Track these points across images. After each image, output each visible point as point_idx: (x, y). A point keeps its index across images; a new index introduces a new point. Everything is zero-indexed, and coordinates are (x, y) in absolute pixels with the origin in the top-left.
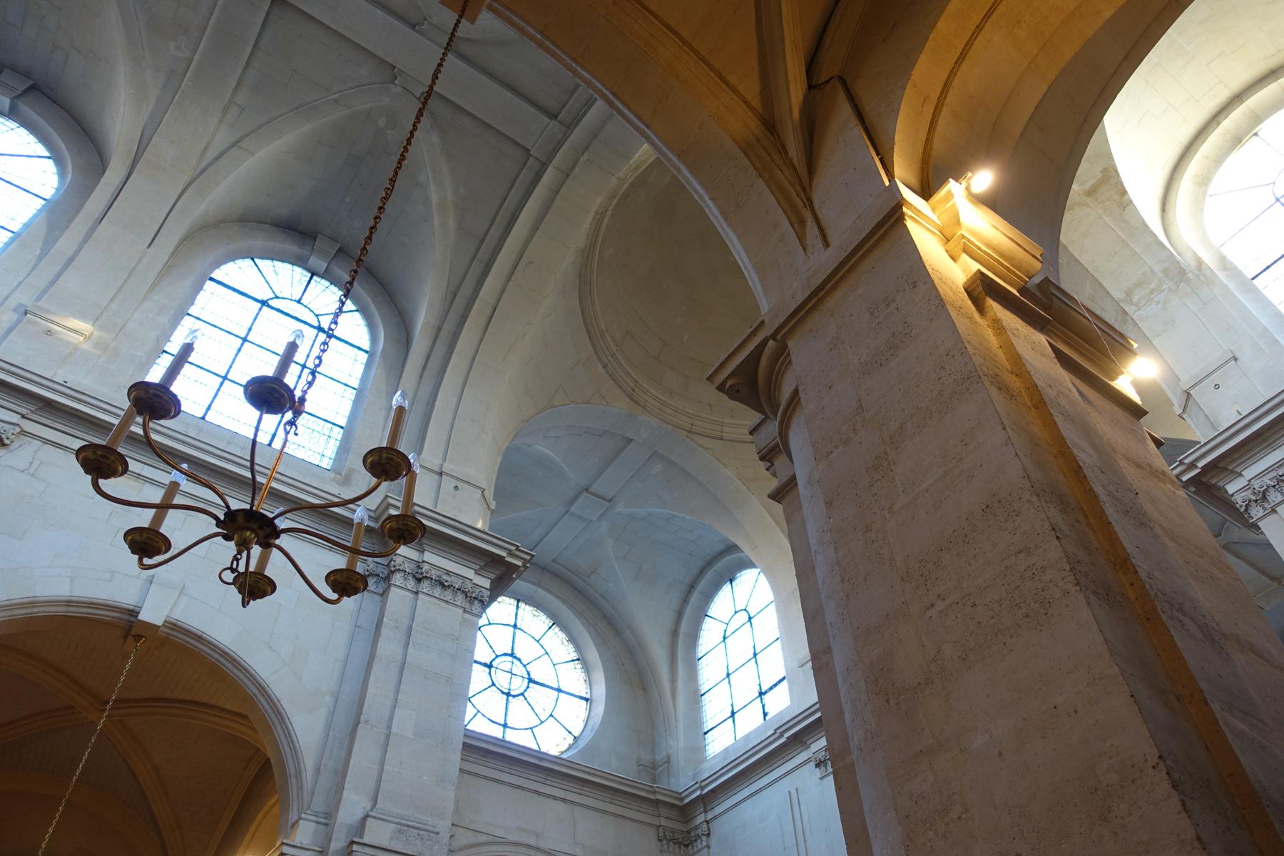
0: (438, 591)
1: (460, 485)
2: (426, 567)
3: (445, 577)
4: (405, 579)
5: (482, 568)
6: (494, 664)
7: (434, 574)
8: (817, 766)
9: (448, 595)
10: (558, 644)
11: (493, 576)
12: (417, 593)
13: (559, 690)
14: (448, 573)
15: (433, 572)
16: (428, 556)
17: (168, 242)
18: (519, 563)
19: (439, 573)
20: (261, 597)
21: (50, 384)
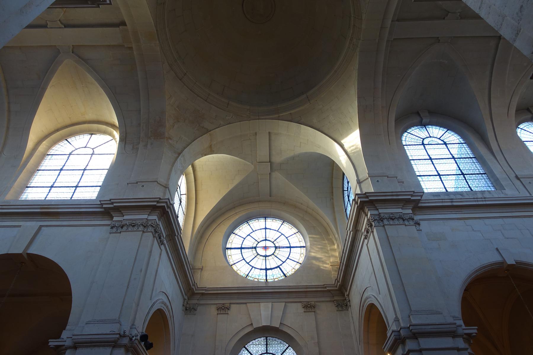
0: (391, 222)
1: (379, 179)
2: (382, 215)
3: (391, 216)
4: (379, 223)
5: (152, 211)
6: (274, 249)
7: (386, 216)
8: (419, 224)
9: (396, 222)
10: (288, 229)
11: (411, 208)
12: (384, 226)
13: (290, 247)
14: (392, 213)
15: (117, 223)
16: (381, 211)
17: (392, 123)
18: (419, 198)
19: (388, 215)
20: (70, 294)
21: (426, 201)
